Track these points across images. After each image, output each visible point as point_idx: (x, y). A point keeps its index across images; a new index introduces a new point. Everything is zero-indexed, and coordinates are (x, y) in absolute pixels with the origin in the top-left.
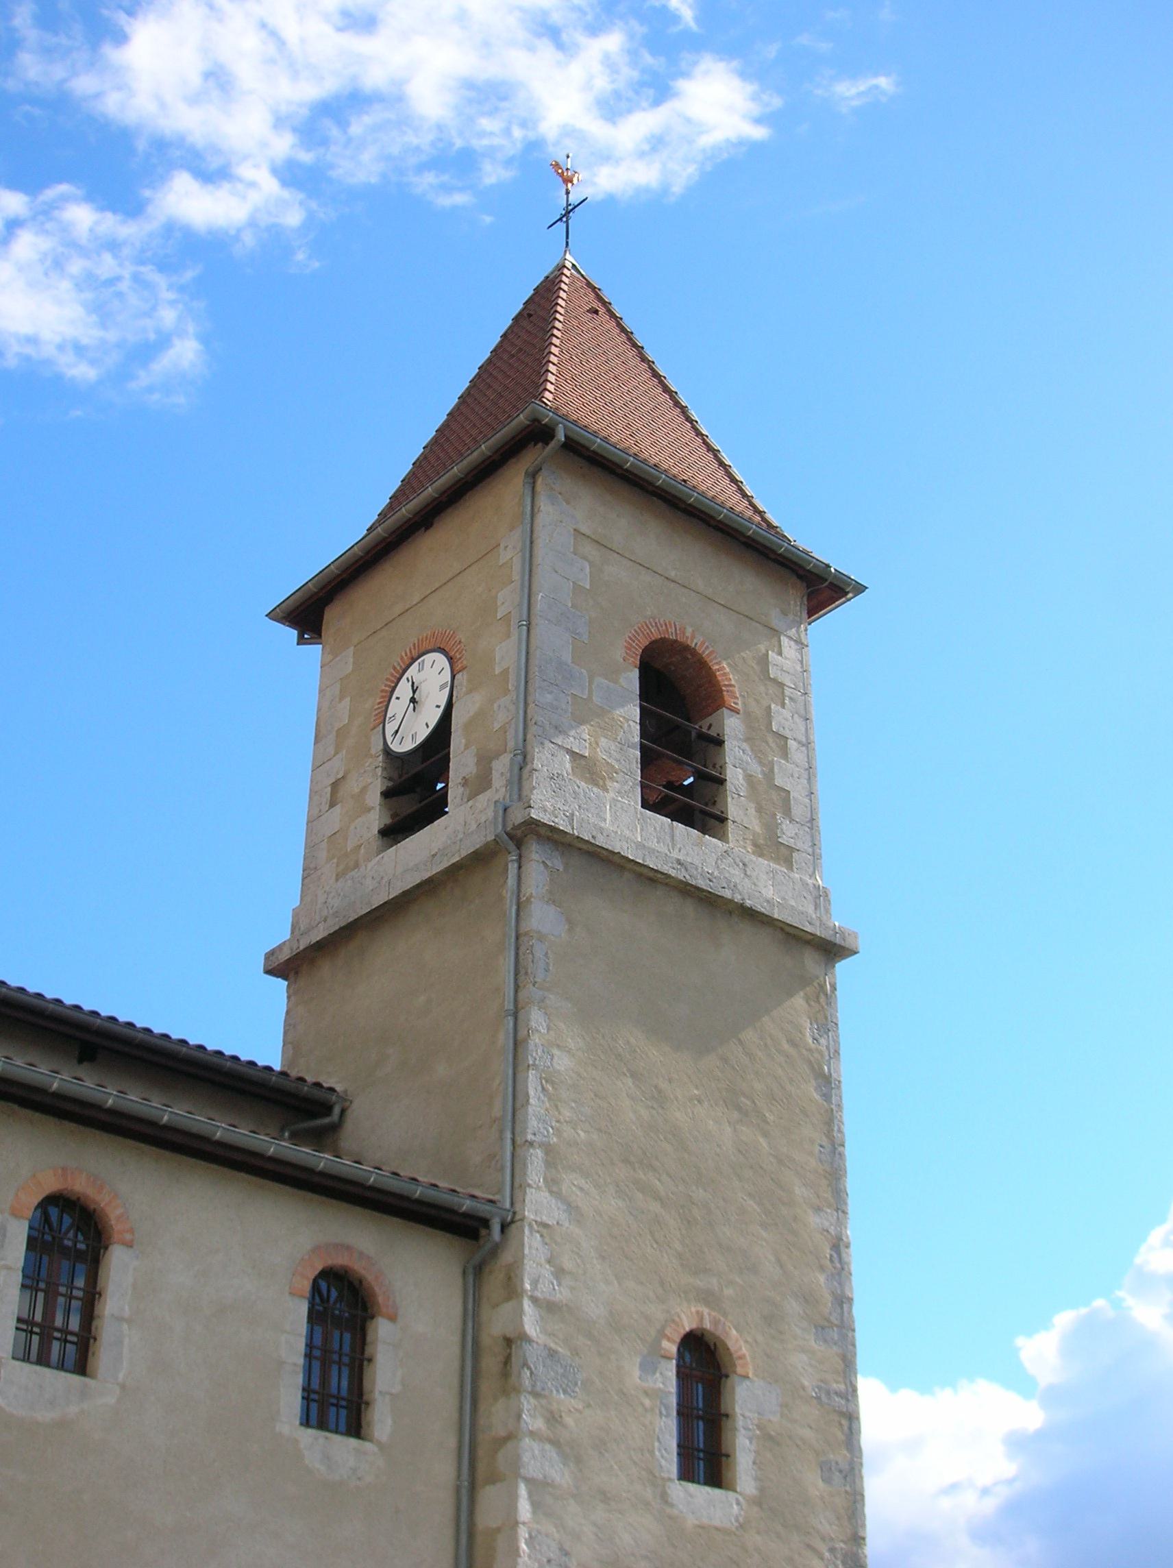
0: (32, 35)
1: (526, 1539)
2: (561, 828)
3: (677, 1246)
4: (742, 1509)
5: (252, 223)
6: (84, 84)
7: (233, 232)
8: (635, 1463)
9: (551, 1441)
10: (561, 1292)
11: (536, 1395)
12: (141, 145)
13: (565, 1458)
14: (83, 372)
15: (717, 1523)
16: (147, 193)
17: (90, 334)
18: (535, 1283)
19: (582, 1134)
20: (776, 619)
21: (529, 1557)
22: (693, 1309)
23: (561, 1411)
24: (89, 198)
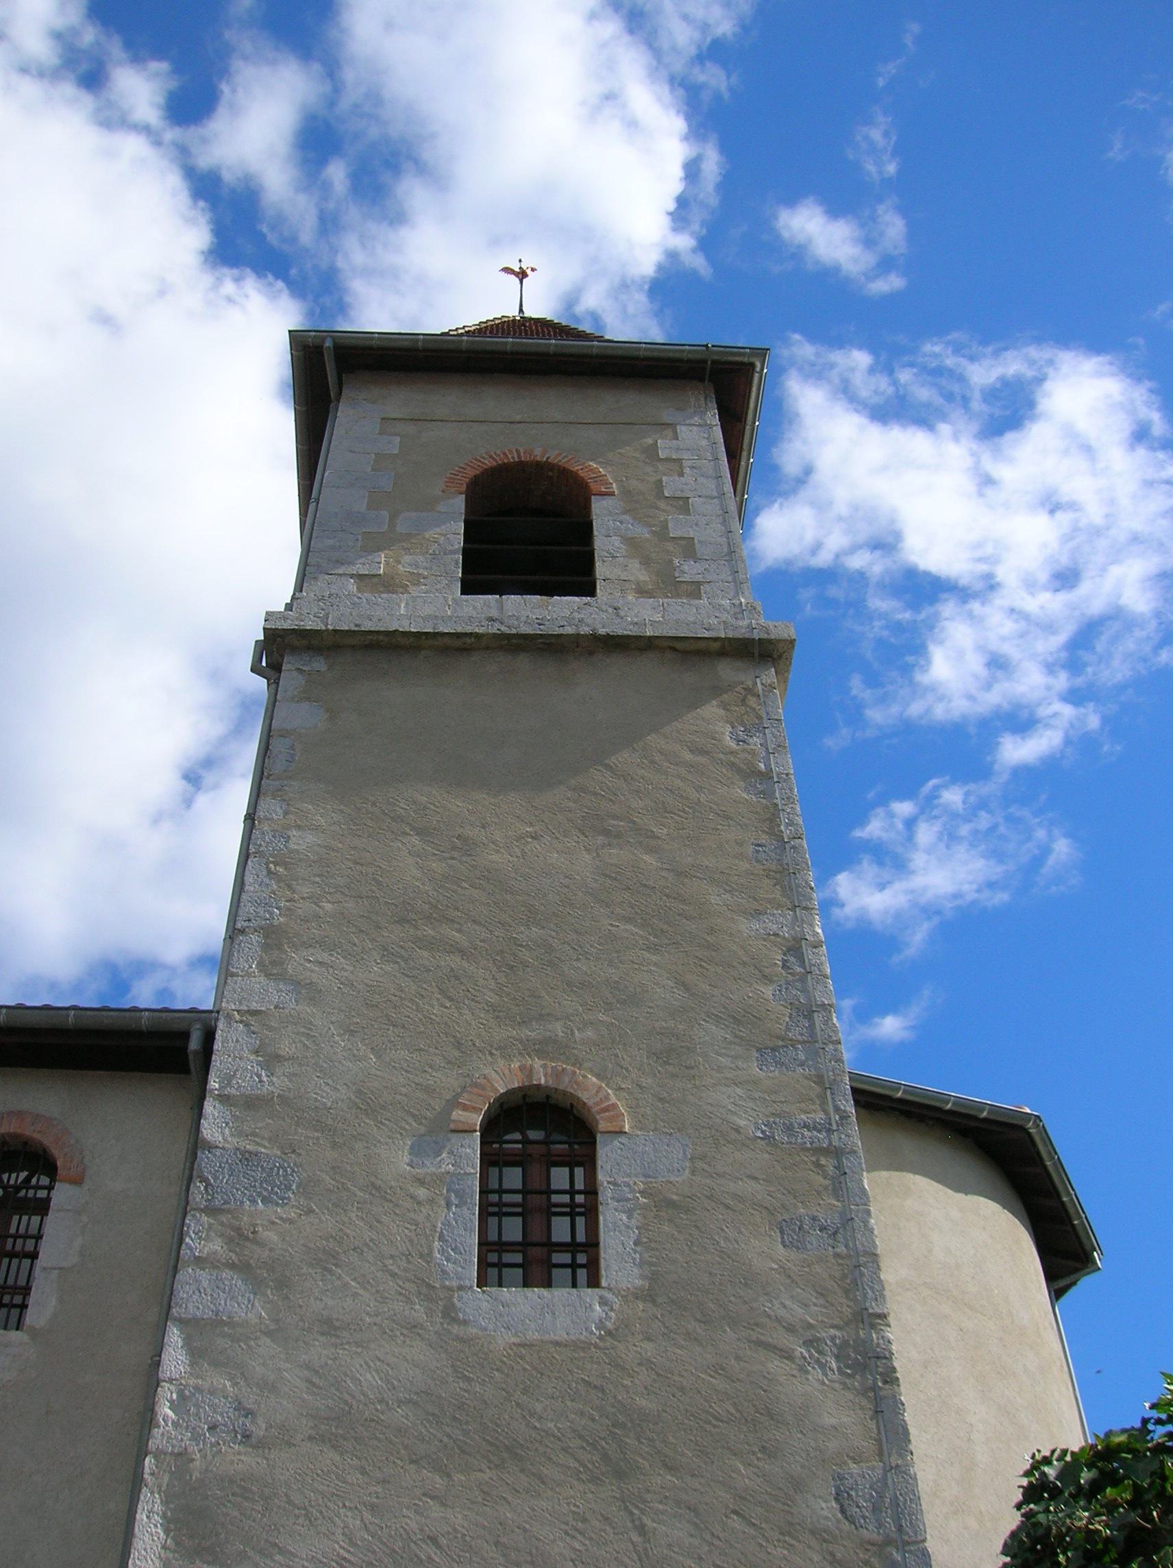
0: (867, 695)
1: (172, 1401)
2: (308, 628)
3: (491, 998)
4: (612, 1309)
5: (1068, 741)
6: (915, 709)
7: (1058, 756)
8: (394, 1275)
9: (232, 1266)
10: (271, 1083)
11: (211, 1211)
12: (972, 730)
13: (257, 1285)
14: (1002, 897)
15: (561, 1336)
16: (989, 758)
17: (996, 870)
18: (227, 1080)
19: (328, 906)
20: (667, 416)
21: (176, 1425)
22: (515, 1065)
23: (255, 1225)
24: (954, 781)
